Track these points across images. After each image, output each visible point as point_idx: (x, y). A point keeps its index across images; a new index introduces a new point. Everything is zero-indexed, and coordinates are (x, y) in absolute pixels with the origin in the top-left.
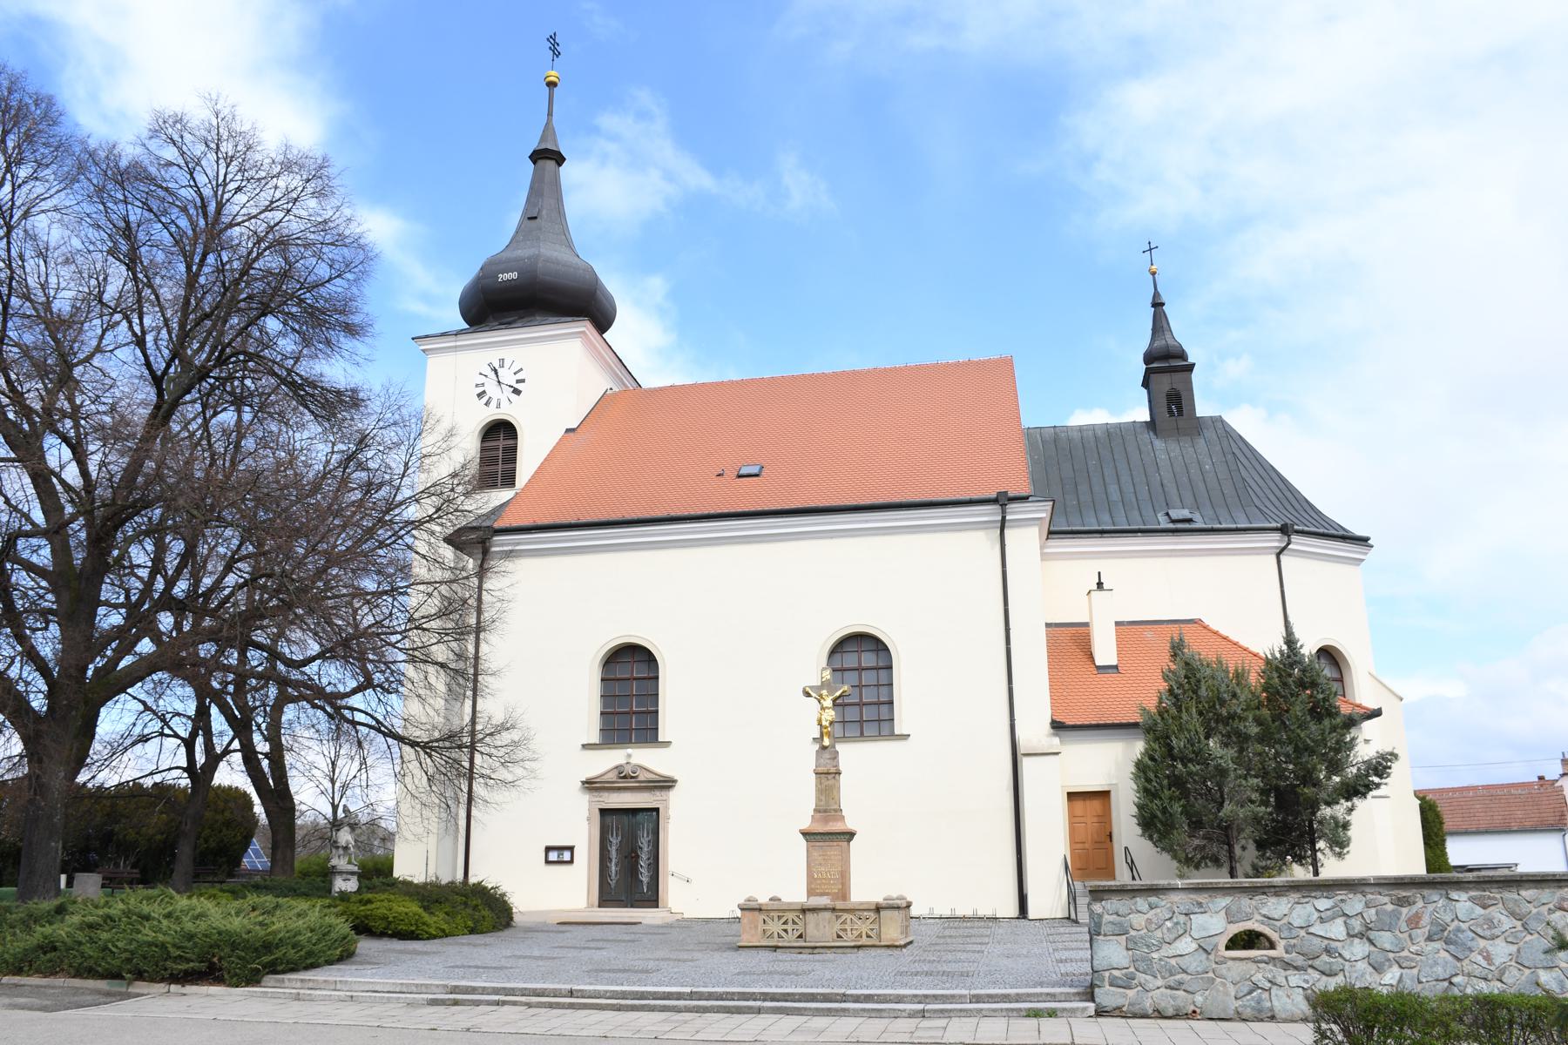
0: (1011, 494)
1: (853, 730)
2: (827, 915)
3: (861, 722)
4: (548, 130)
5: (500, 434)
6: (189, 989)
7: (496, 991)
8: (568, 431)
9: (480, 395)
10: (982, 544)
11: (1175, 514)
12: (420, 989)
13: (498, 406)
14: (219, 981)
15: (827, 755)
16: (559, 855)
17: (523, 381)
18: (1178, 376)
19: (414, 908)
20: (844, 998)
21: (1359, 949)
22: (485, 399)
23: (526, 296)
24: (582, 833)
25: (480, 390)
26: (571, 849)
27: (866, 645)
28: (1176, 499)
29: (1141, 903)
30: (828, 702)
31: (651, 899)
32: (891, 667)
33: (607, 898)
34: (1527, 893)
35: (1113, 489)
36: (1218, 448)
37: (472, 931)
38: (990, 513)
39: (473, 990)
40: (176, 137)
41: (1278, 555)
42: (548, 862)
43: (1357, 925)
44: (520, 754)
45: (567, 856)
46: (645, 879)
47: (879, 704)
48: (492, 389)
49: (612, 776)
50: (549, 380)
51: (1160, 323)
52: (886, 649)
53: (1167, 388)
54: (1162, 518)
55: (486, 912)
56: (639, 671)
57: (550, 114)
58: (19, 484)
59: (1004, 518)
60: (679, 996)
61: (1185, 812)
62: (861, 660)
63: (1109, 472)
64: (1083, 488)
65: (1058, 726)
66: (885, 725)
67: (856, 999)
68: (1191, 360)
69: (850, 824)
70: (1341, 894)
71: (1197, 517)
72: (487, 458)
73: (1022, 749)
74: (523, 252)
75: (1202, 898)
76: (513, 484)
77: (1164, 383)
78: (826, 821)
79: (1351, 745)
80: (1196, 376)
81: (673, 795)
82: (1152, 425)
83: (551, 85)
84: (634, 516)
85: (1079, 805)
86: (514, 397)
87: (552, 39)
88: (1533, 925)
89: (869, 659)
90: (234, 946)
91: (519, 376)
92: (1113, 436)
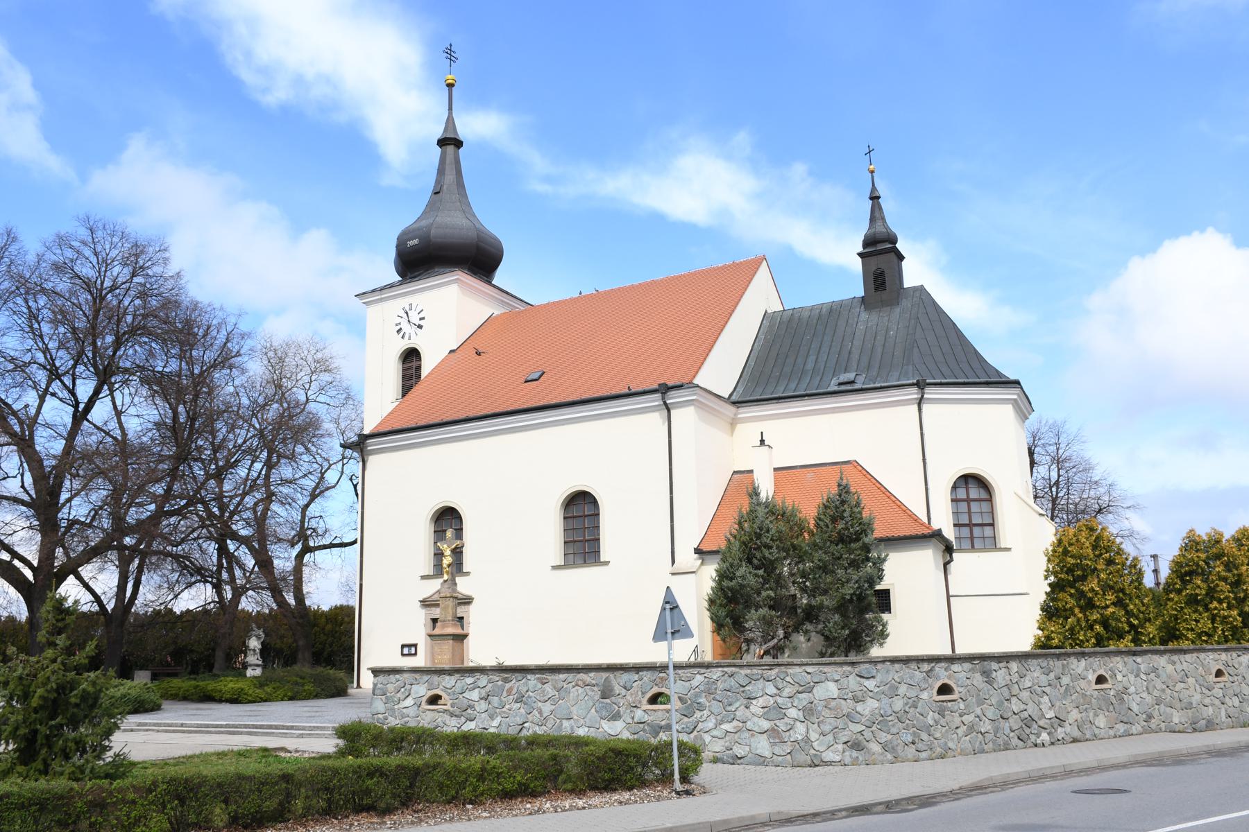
0: (670, 384)
1: (579, 560)
4: (450, 122)
5: (411, 356)
8: (451, 352)
9: (399, 331)
10: (656, 420)
21: (483, 706)
26: (415, 646)
28: (854, 364)
34: (562, 676)
35: (812, 358)
37: (291, 699)
38: (655, 400)
42: (403, 655)
43: (483, 693)
48: (406, 328)
51: (876, 212)
52: (460, 518)
53: (873, 268)
56: (588, 510)
58: (12, 461)
61: (821, 607)
62: (581, 511)
63: (815, 345)
70: (478, 675)
75: (417, 676)
77: (875, 262)
81: (472, 608)
84: (479, 414)
91: (421, 315)
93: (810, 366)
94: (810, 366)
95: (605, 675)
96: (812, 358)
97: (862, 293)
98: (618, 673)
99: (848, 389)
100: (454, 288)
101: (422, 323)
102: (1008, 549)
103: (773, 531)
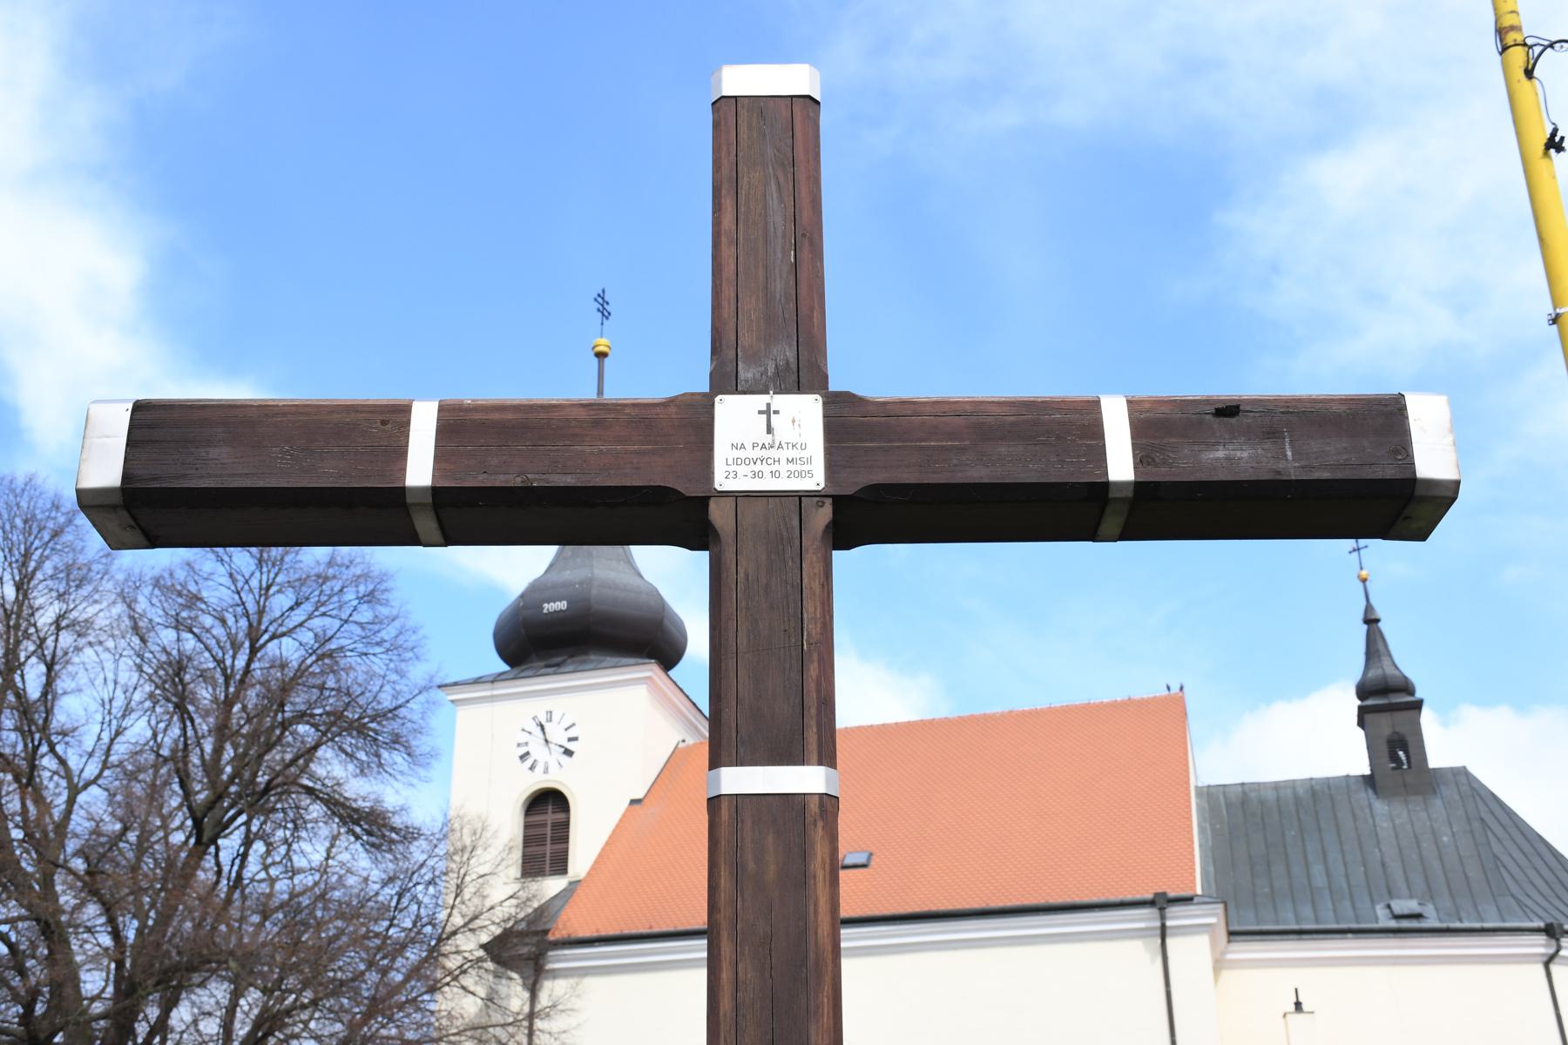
0: (1172, 894)
5: (548, 805)
8: (633, 802)
9: (523, 757)
10: (1138, 956)
11: (1400, 906)
13: (546, 771)
17: (575, 739)
22: (529, 762)
25: (523, 750)
35: (1318, 870)
36: (1461, 812)
38: (1145, 919)
40: (478, 923)
41: (1547, 965)
54: (1381, 911)
59: (1163, 928)
64: (1279, 869)
68: (1419, 695)
71: (1429, 910)
72: (531, 839)
77: (1385, 724)
80: (1427, 719)
82: (1369, 781)
83: (601, 356)
86: (565, 758)
87: (605, 314)
91: (571, 733)
92: (1315, 801)
93: (1320, 880)
94: (1320, 880)
96: (1318, 870)
97: (1367, 772)
99: (1408, 927)
100: (641, 691)
101: (571, 746)
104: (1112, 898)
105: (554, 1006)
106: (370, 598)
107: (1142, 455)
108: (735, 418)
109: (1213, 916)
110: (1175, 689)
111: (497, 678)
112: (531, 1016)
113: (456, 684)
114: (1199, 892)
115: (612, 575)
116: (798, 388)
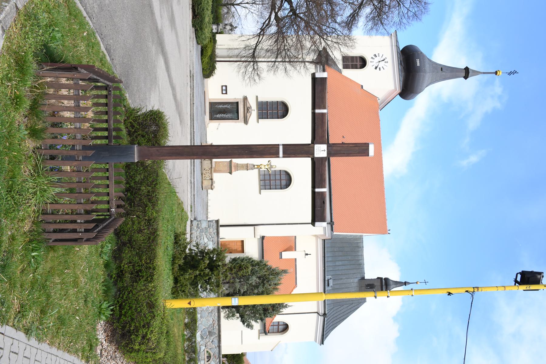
0: (333, 226)
1: (262, 178)
2: (210, 166)
3: (265, 180)
4: (476, 73)
5: (361, 63)
6: (191, 10)
7: (193, 86)
8: (362, 86)
9: (375, 55)
11: (331, 281)
12: (193, 67)
13: (371, 62)
14: (193, 18)
15: (252, 167)
16: (224, 90)
18: (380, 288)
19: (209, 54)
20: (194, 166)
22: (374, 57)
23: (411, 69)
24: (230, 97)
25: (377, 55)
26: (226, 93)
27: (288, 182)
28: (336, 283)
29: (215, 231)
30: (266, 167)
31: (212, 118)
32: (281, 189)
33: (212, 104)
34: (216, 314)
35: (340, 263)
37: (203, 69)
39: (193, 81)
42: (222, 86)
44: (252, 81)
45: (224, 92)
46: (218, 116)
47: (270, 185)
49: (248, 105)
50: (381, 79)
51: (398, 284)
53: (376, 284)
54: (330, 277)
55: (208, 72)
56: (280, 113)
57: (484, 73)
60: (193, 129)
64: (341, 254)
65: (263, 238)
66: (264, 187)
67: (194, 169)
69: (234, 173)
71: (330, 288)
72: (353, 58)
73: (256, 227)
74: (427, 67)
76: (344, 68)
77: (378, 284)
78: (235, 166)
79: (256, 321)
81: (243, 124)
82: (363, 278)
83: (496, 73)
85: (240, 244)
87: (510, 74)
88: (210, 314)
89: (284, 183)
90: (201, 21)
91: (382, 69)
92: (359, 265)
93: (337, 263)
94: (337, 263)
95: (217, 332)
96: (340, 263)
98: (217, 338)
100: (393, 88)
101: (378, 68)
102: (259, 338)
103: (269, 287)
104: (333, 212)
105: (307, 69)
106: (415, 14)
107: (318, 193)
108: (324, 147)
109: (328, 236)
110: (389, 232)
111: (398, 47)
112: (304, 62)
113: (396, 35)
114: (334, 233)
115: (427, 78)
116: (328, 154)
